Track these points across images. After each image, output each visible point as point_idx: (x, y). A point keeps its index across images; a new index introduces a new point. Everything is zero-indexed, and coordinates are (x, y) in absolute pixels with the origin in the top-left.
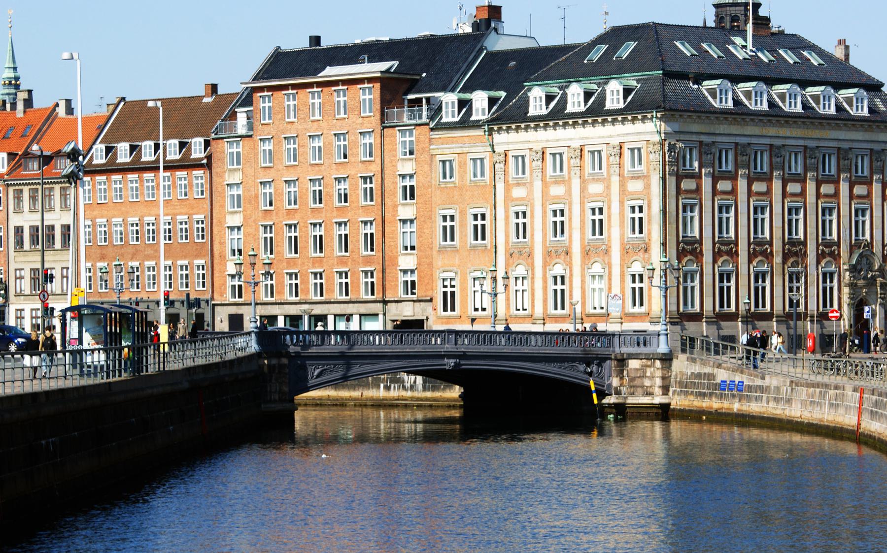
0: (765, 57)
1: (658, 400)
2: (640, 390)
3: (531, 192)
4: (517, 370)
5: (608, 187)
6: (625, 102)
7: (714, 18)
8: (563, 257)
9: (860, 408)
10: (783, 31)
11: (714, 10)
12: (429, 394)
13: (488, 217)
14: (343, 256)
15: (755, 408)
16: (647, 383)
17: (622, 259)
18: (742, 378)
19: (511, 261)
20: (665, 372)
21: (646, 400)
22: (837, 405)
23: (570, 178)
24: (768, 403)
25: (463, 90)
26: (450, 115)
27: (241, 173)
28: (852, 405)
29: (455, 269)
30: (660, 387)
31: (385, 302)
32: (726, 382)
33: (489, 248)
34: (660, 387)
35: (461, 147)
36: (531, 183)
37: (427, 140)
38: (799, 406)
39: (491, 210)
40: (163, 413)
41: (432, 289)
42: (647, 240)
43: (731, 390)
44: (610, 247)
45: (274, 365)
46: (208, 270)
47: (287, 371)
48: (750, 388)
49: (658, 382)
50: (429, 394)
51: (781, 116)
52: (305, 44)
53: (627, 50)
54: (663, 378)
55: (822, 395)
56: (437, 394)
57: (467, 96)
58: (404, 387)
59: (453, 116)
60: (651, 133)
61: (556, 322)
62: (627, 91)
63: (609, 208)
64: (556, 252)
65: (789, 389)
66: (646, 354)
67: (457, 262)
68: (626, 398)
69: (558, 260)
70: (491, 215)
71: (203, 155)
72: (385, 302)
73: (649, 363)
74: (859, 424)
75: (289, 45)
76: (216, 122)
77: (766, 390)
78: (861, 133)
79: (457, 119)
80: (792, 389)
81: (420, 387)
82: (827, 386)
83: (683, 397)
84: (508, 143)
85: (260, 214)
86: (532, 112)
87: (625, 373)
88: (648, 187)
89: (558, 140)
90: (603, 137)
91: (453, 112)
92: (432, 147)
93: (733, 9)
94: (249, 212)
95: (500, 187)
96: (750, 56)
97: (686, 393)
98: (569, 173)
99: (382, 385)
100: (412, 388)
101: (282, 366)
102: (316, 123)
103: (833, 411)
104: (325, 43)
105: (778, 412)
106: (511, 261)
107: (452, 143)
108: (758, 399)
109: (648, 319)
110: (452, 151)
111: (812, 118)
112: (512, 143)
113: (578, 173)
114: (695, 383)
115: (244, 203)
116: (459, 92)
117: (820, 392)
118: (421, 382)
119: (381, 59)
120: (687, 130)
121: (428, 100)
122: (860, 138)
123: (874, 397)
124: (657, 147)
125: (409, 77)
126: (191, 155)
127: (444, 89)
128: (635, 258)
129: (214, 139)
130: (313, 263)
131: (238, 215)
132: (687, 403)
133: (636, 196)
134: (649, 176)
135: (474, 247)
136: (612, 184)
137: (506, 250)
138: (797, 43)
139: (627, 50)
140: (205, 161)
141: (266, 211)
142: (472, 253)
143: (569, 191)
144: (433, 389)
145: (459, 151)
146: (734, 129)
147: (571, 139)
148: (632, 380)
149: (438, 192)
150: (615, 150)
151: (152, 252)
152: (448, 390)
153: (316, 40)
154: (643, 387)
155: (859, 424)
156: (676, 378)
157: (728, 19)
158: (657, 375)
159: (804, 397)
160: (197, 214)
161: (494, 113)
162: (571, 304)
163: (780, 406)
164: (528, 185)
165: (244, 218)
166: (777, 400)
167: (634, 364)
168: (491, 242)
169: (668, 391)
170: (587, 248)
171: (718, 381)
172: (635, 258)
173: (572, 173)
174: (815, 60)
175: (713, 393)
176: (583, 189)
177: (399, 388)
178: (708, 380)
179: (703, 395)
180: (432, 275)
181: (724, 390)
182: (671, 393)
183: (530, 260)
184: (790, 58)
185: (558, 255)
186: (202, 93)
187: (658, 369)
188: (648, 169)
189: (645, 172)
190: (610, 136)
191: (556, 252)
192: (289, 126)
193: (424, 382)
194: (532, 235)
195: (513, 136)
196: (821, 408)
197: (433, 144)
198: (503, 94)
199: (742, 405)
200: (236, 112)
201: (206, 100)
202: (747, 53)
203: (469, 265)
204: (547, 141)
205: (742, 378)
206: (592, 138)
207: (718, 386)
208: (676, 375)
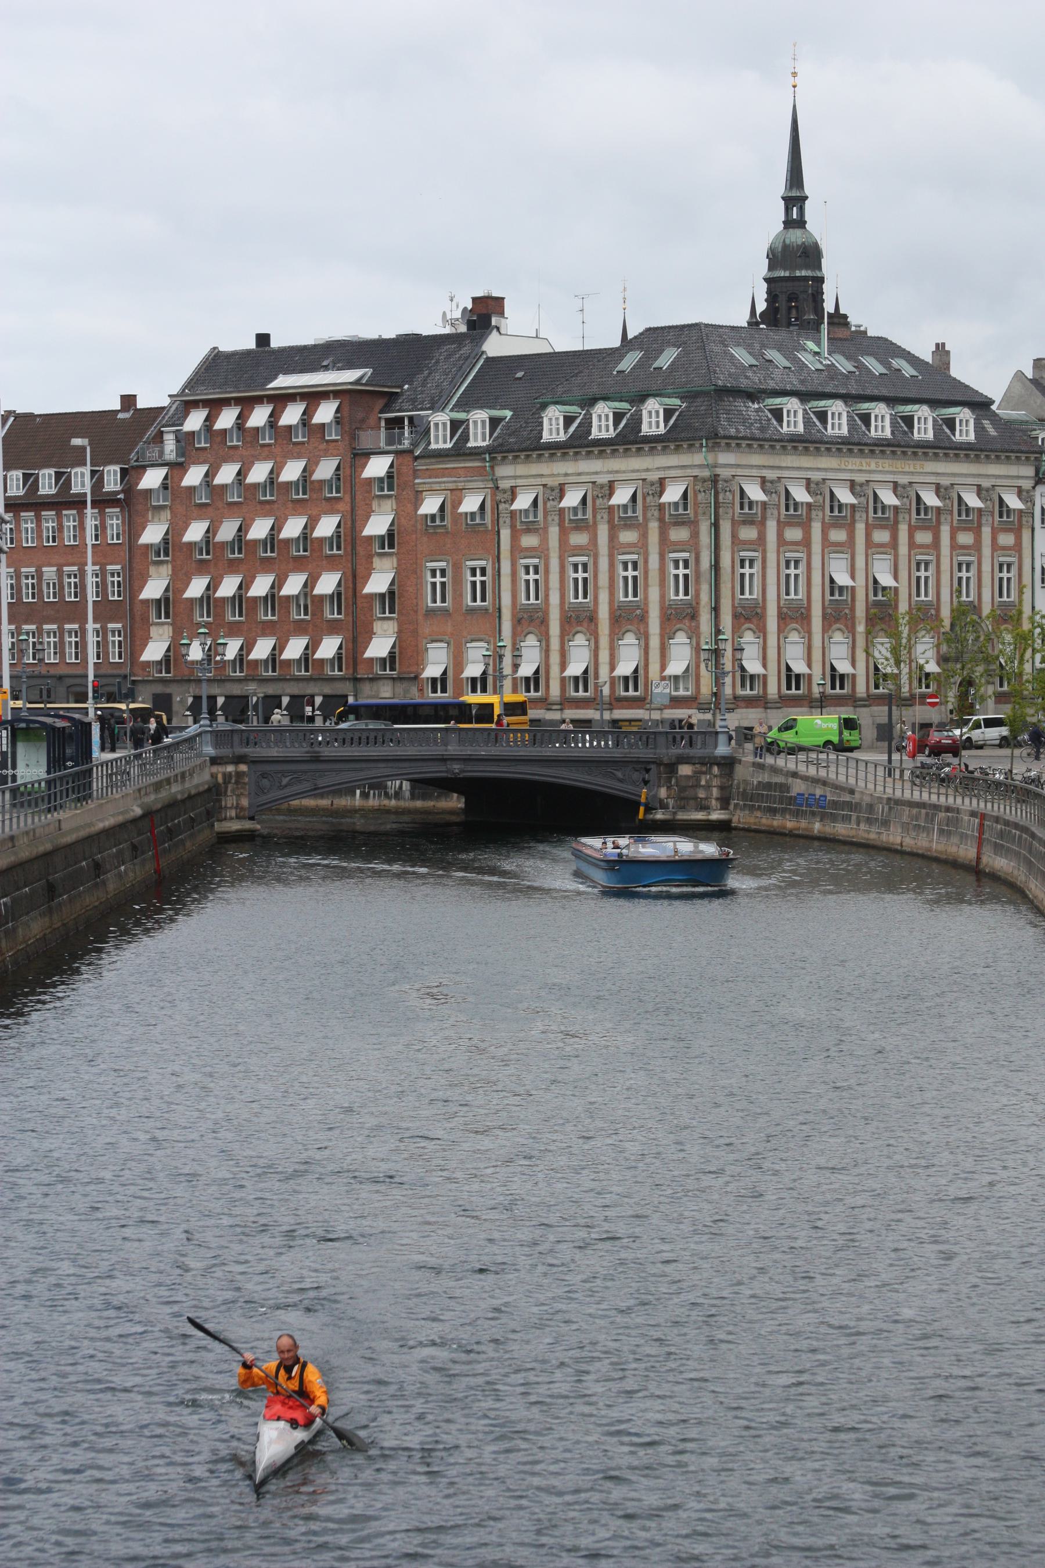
0: (844, 365)
1: (716, 816)
2: (692, 802)
3: (545, 540)
4: (537, 777)
5: (644, 536)
6: (665, 426)
7: (765, 296)
8: (585, 624)
9: (980, 838)
10: (865, 332)
11: (765, 285)
12: (419, 804)
13: (489, 571)
14: (302, 620)
15: (841, 829)
16: (702, 794)
17: (662, 628)
18: (825, 791)
19: (519, 629)
20: (725, 780)
21: (700, 816)
22: (949, 833)
23: (595, 523)
24: (858, 825)
25: (458, 407)
26: (440, 441)
27: (169, 512)
28: (969, 833)
29: (447, 638)
30: (717, 799)
31: (356, 680)
32: (803, 795)
33: (491, 611)
34: (717, 799)
35: (455, 482)
36: (546, 529)
37: (411, 472)
38: (900, 830)
39: (493, 563)
40: (114, 850)
41: (417, 664)
42: (694, 603)
43: (810, 806)
44: (647, 612)
45: (230, 773)
46: (125, 637)
47: (246, 780)
48: (835, 804)
49: (715, 792)
50: (419, 804)
51: (866, 444)
52: (251, 344)
53: (667, 359)
54: (722, 788)
55: (930, 818)
56: (429, 804)
57: (462, 416)
58: (387, 795)
59: (445, 442)
60: (700, 466)
61: (577, 708)
62: (668, 413)
63: (646, 562)
64: (578, 617)
65: (886, 808)
66: (700, 758)
67: (449, 628)
68: (675, 813)
69: (579, 628)
70: (493, 568)
71: (118, 488)
72: (356, 680)
73: (704, 769)
74: (979, 858)
75: (227, 346)
76: (137, 445)
77: (856, 808)
78: (966, 465)
79: (449, 445)
80: (890, 809)
81: (407, 794)
82: (936, 807)
83: (747, 812)
84: (515, 477)
85: (194, 565)
86: (546, 437)
87: (673, 781)
88: (695, 535)
89: (579, 474)
90: (638, 471)
91: (445, 436)
92: (417, 481)
93: (790, 284)
94: (179, 562)
95: (505, 534)
96: (824, 365)
97: (752, 808)
98: (594, 516)
99: (358, 792)
100: (398, 795)
101: (239, 775)
102: (266, 449)
103: (943, 840)
104: (275, 344)
105: (872, 836)
106: (519, 629)
107: (443, 476)
108: (847, 819)
109: (695, 705)
110: (443, 486)
111: (903, 447)
112: (520, 477)
113: (606, 516)
114: (763, 795)
115: (173, 550)
116: (452, 410)
117: (927, 814)
118: (409, 788)
119: (350, 365)
120: (744, 462)
121: (411, 419)
122: (965, 471)
123: (999, 826)
124: (709, 484)
125: (386, 390)
126: (103, 487)
127: (433, 407)
128: (678, 626)
129: (133, 467)
130: (263, 629)
131: (165, 566)
132: (752, 820)
133: (681, 547)
134: (697, 522)
135: (472, 611)
136: (650, 532)
137: (513, 615)
138: (885, 349)
139: (667, 359)
140: (121, 496)
141: (202, 561)
142: (469, 617)
143: (594, 540)
144: (424, 797)
145: (451, 486)
146: (806, 461)
147: (596, 473)
148: (681, 789)
149: (425, 539)
150: (653, 488)
151: (52, 613)
152: (443, 799)
153: (263, 339)
154: (696, 798)
155: (979, 858)
156: (738, 788)
157: (783, 298)
158: (714, 784)
159: (905, 819)
160: (111, 564)
161: (497, 437)
162: (596, 685)
163: (874, 829)
164: (541, 531)
165: (173, 570)
166: (869, 821)
167: (685, 770)
168: (494, 604)
169: (728, 804)
170: (618, 613)
171: (793, 793)
172: (678, 626)
173: (599, 517)
174: (908, 371)
175: (786, 809)
176: (612, 538)
177: (380, 796)
178: (781, 792)
179: (773, 811)
180: (417, 646)
181: (801, 805)
182: (732, 807)
183: (543, 628)
184: (875, 367)
185: (579, 622)
186: (117, 406)
187: (715, 776)
188: (696, 513)
189: (692, 516)
190: (647, 470)
191: (578, 617)
192: (232, 452)
193: (413, 788)
194: (547, 596)
195: (521, 469)
196: (928, 834)
197: (418, 478)
198: (508, 414)
199: (824, 825)
200: (162, 432)
201: (120, 416)
202: (821, 363)
203: (465, 634)
204: (566, 475)
205: (825, 791)
206: (624, 472)
207: (792, 800)
208: (739, 784)
